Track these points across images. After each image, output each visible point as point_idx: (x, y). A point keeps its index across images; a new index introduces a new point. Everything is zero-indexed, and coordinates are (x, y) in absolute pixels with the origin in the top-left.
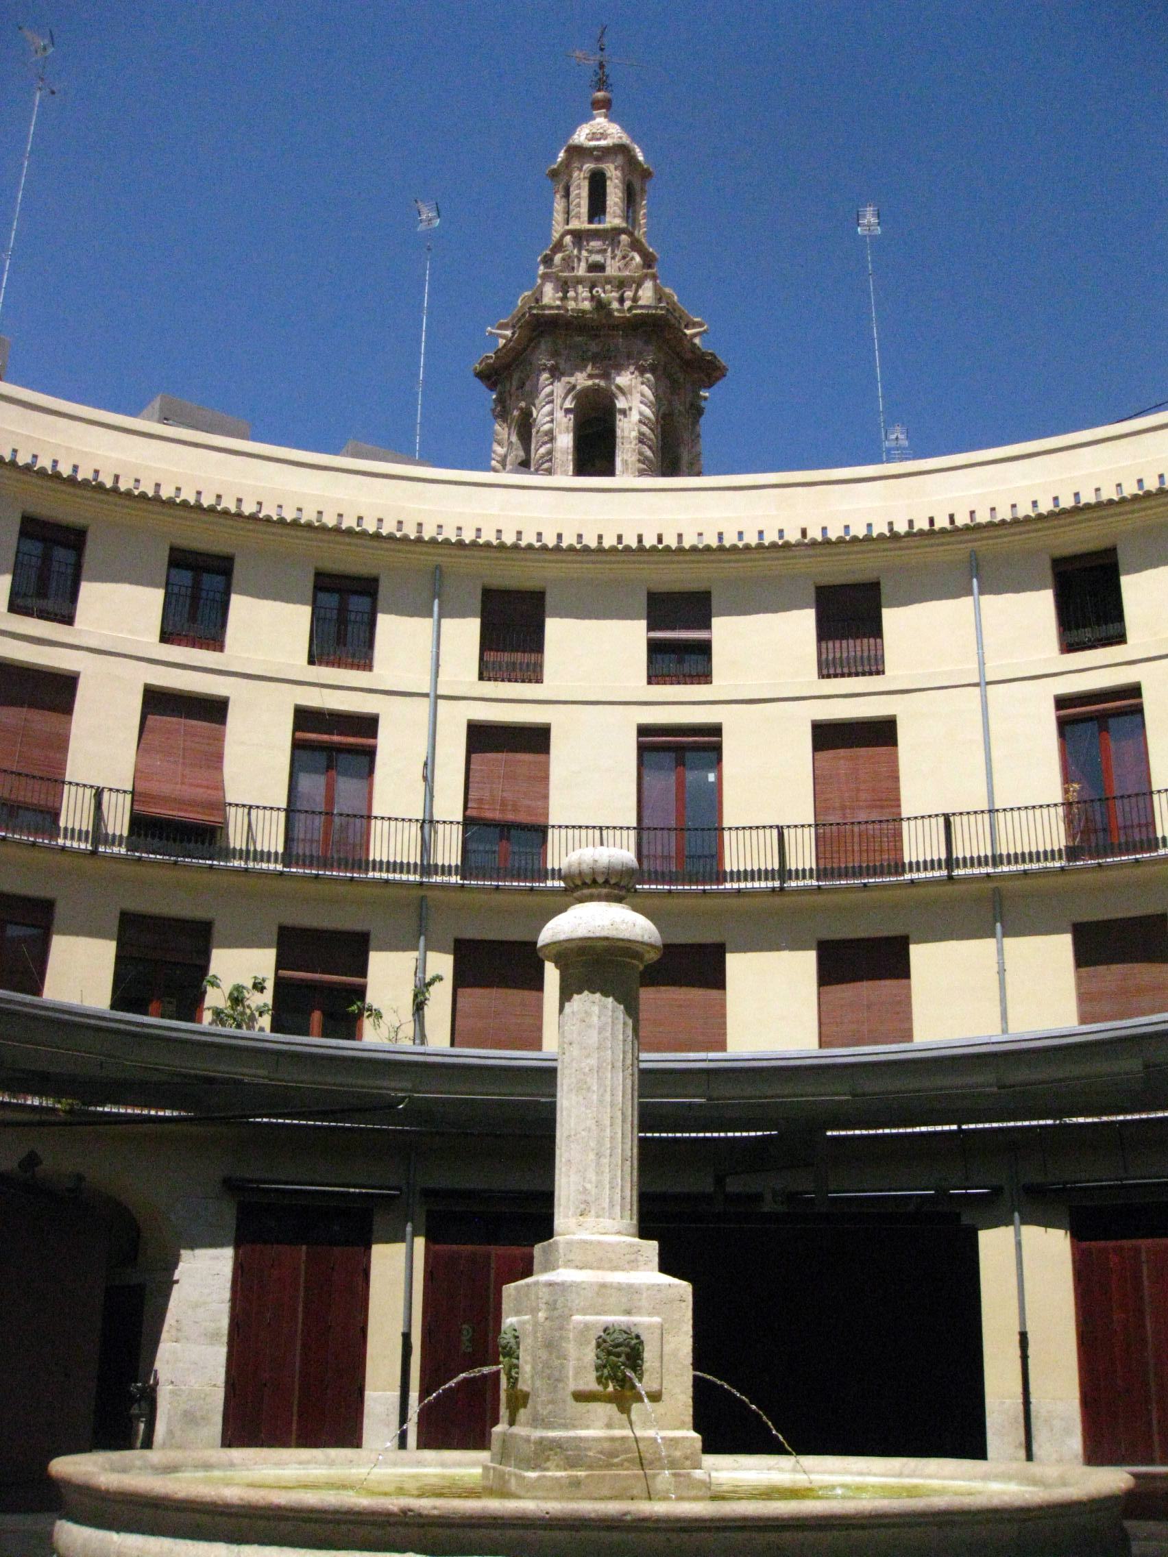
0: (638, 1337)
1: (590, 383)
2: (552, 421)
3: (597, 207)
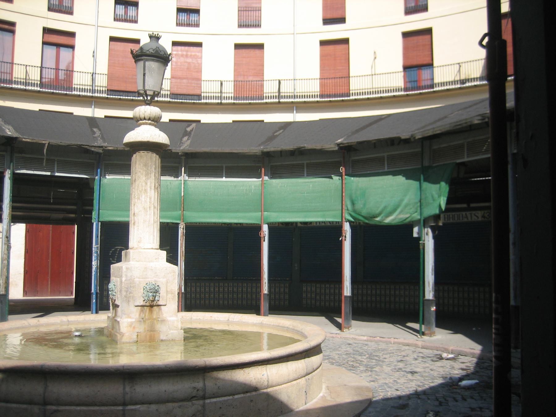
0: (158, 286)
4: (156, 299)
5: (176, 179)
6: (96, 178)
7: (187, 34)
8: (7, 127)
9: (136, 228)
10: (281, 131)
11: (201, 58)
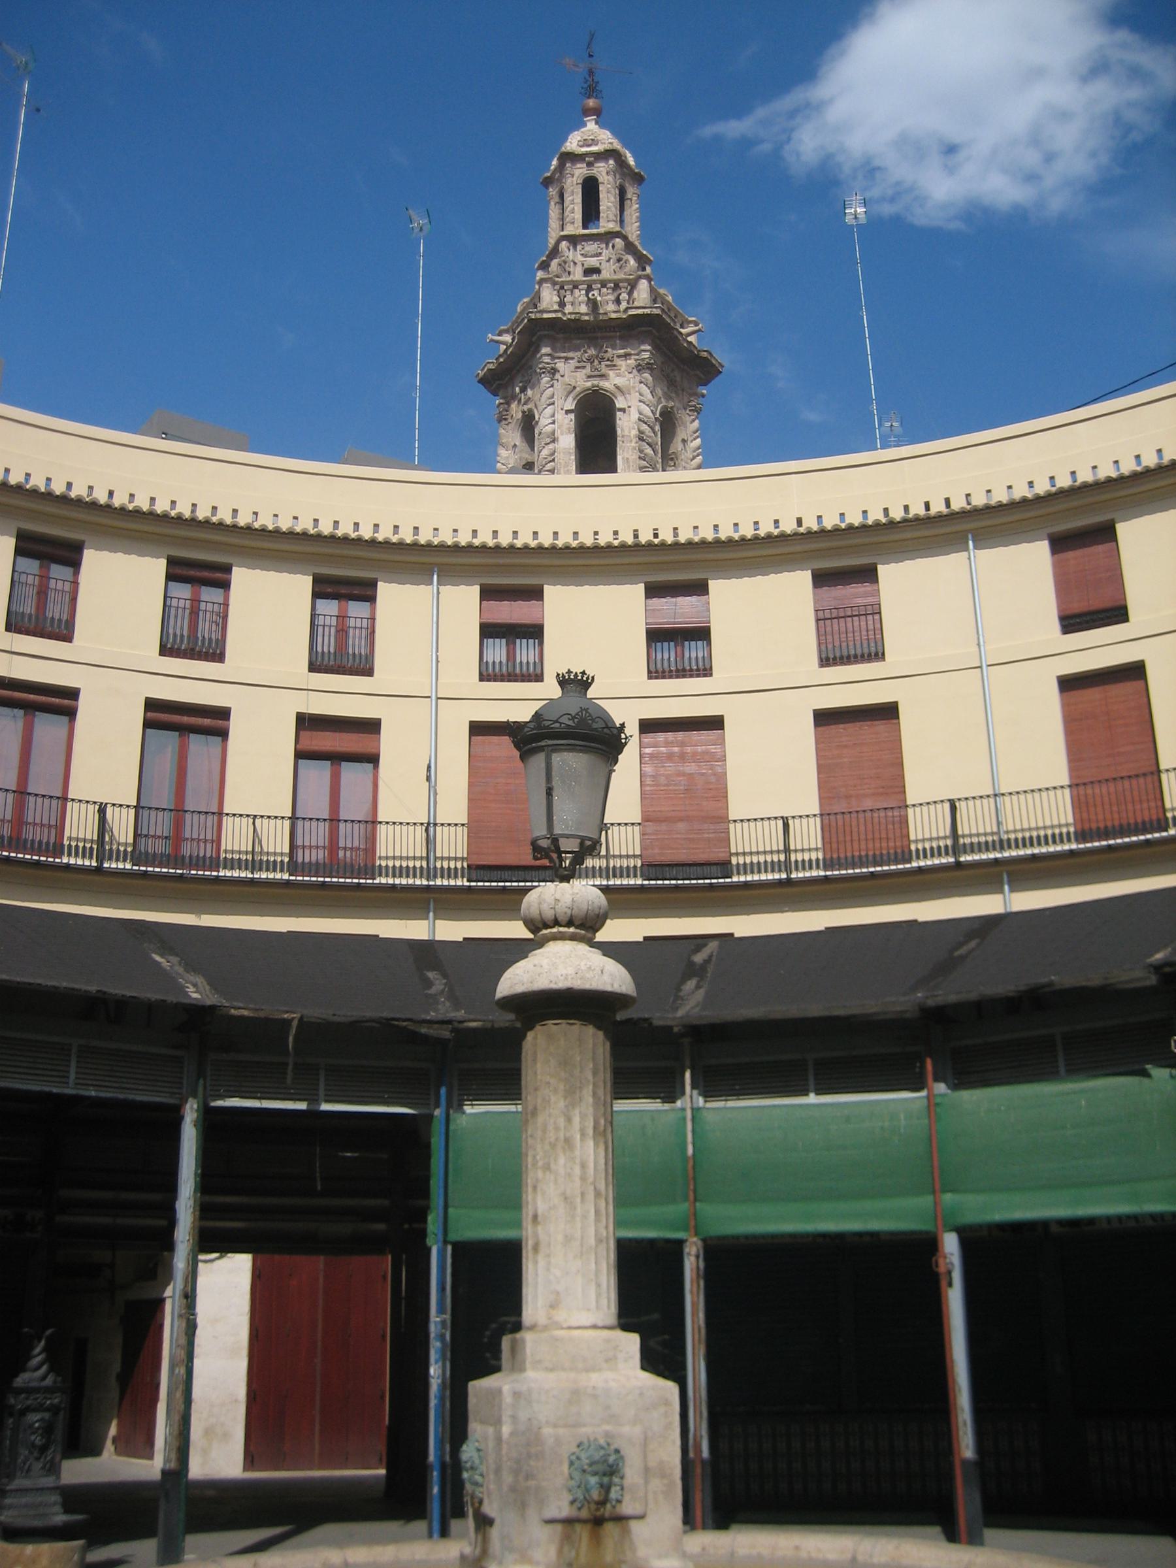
0: (617, 1451)
1: (589, 384)
2: (554, 423)
3: (591, 212)
4: (613, 1495)
5: (667, 1106)
6: (437, 1112)
7: (680, 698)
8: (192, 978)
9: (542, 1263)
10: (973, 944)
11: (723, 759)
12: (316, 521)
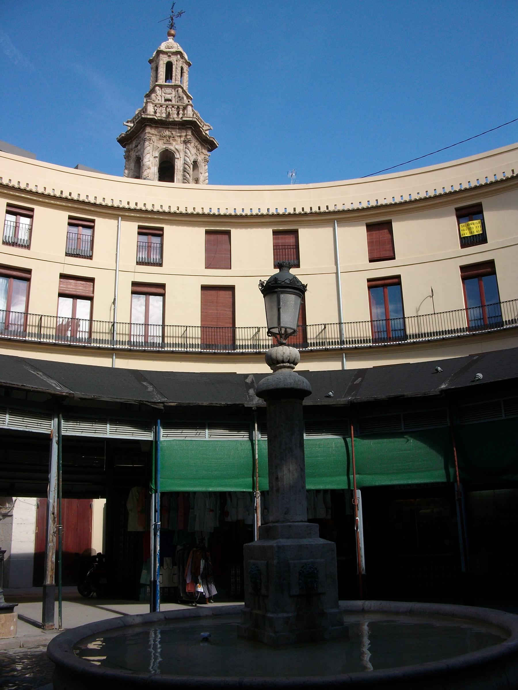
1: (164, 147)
12: (87, 196)
